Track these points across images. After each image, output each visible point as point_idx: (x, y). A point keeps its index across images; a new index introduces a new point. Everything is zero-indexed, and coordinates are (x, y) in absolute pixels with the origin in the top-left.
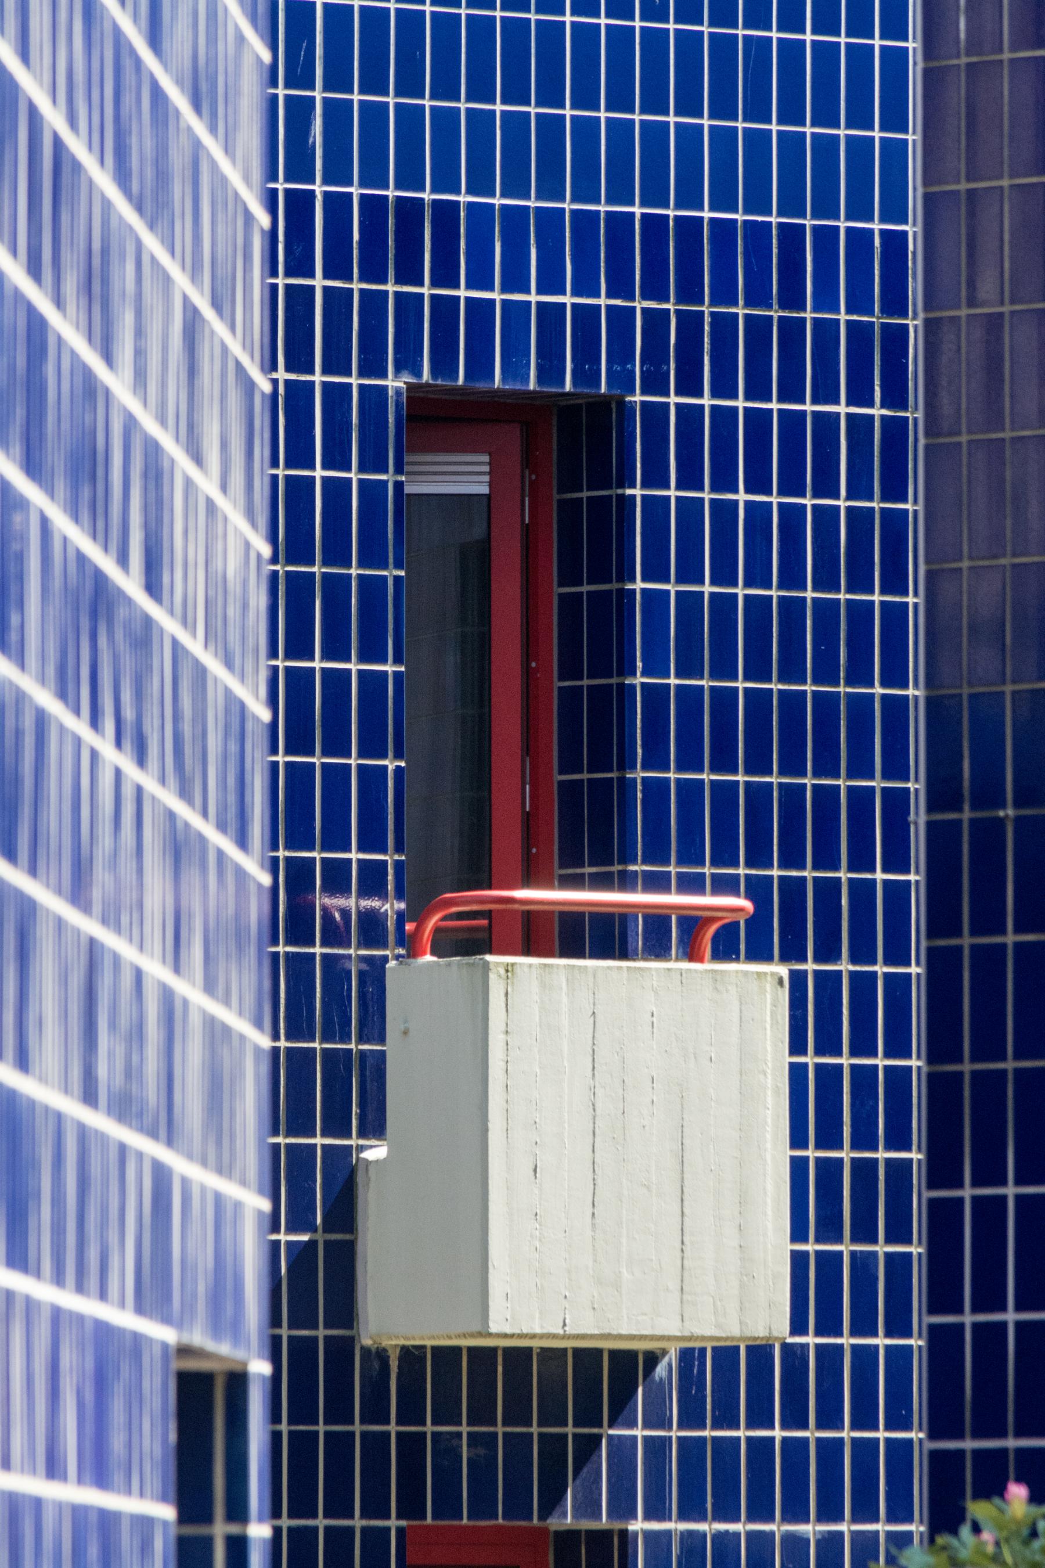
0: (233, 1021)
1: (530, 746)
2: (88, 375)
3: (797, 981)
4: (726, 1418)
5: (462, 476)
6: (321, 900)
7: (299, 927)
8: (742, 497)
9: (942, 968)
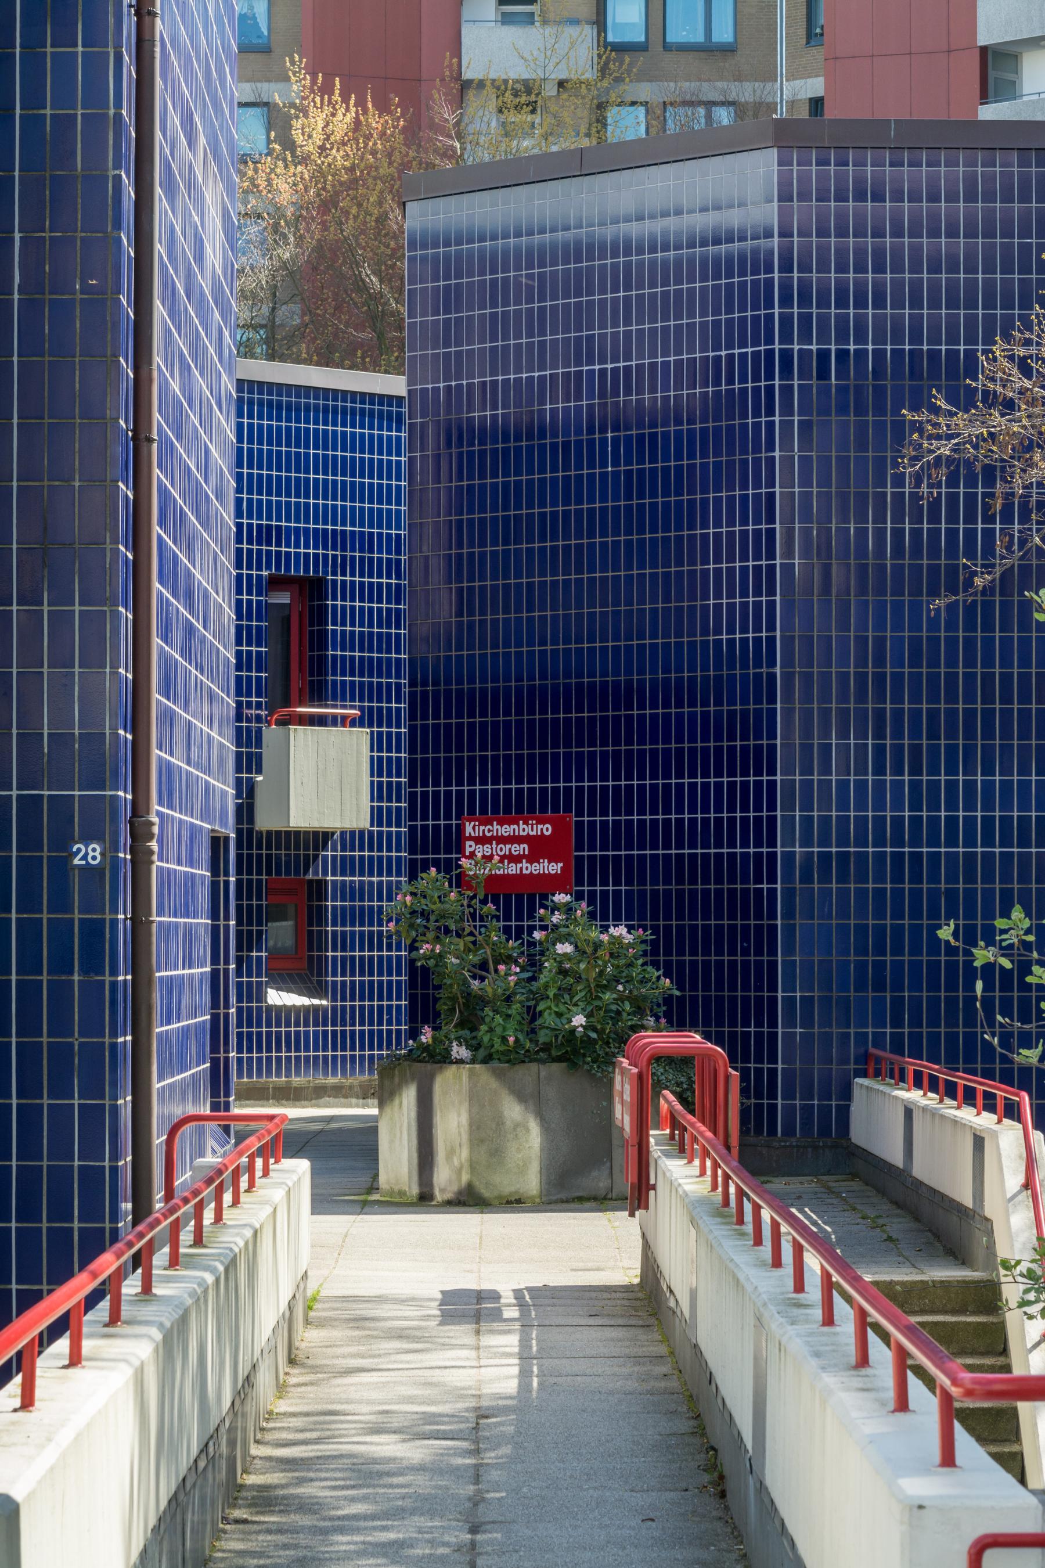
0: (224, 742)
1: (301, 670)
2: (189, 570)
3: (372, 733)
4: (353, 849)
5: (283, 598)
6: (245, 711)
7: (239, 717)
8: (357, 604)
9: (412, 729)
